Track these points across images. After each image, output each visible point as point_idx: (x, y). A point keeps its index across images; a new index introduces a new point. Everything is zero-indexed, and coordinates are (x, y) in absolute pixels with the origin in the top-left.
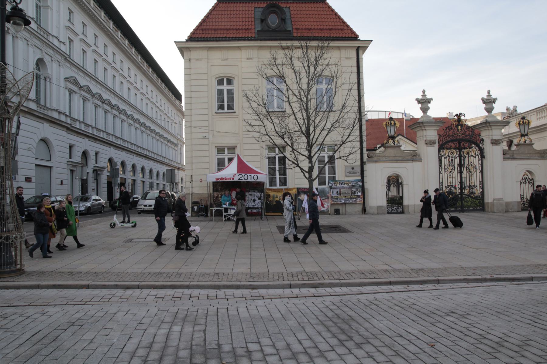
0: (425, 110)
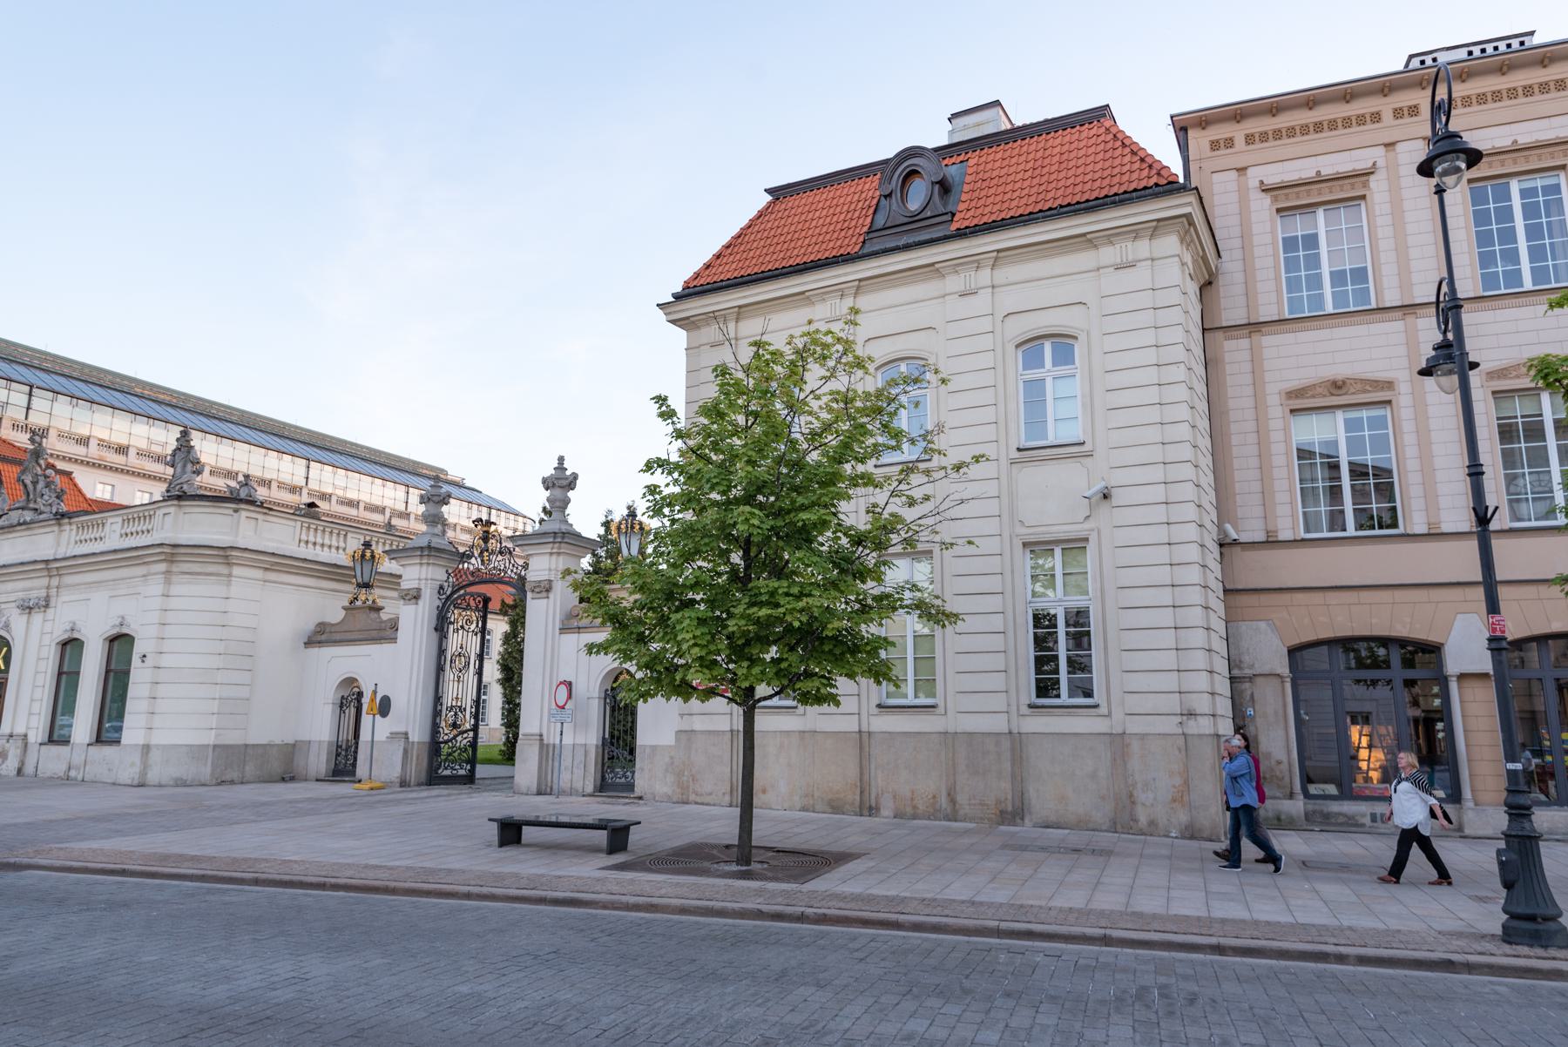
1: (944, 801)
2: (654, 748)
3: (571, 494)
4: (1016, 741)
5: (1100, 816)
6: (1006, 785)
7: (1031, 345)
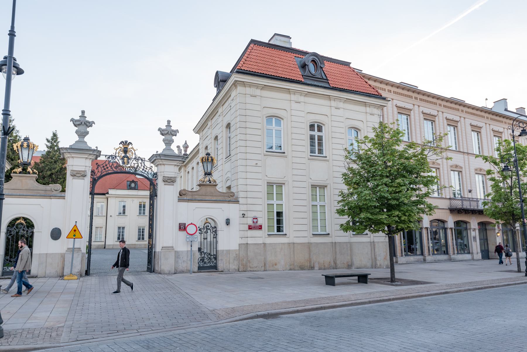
0: (82, 134)
1: (332, 263)
2: (228, 252)
3: (89, 129)
4: (350, 243)
5: (369, 264)
6: (349, 257)
7: (270, 117)
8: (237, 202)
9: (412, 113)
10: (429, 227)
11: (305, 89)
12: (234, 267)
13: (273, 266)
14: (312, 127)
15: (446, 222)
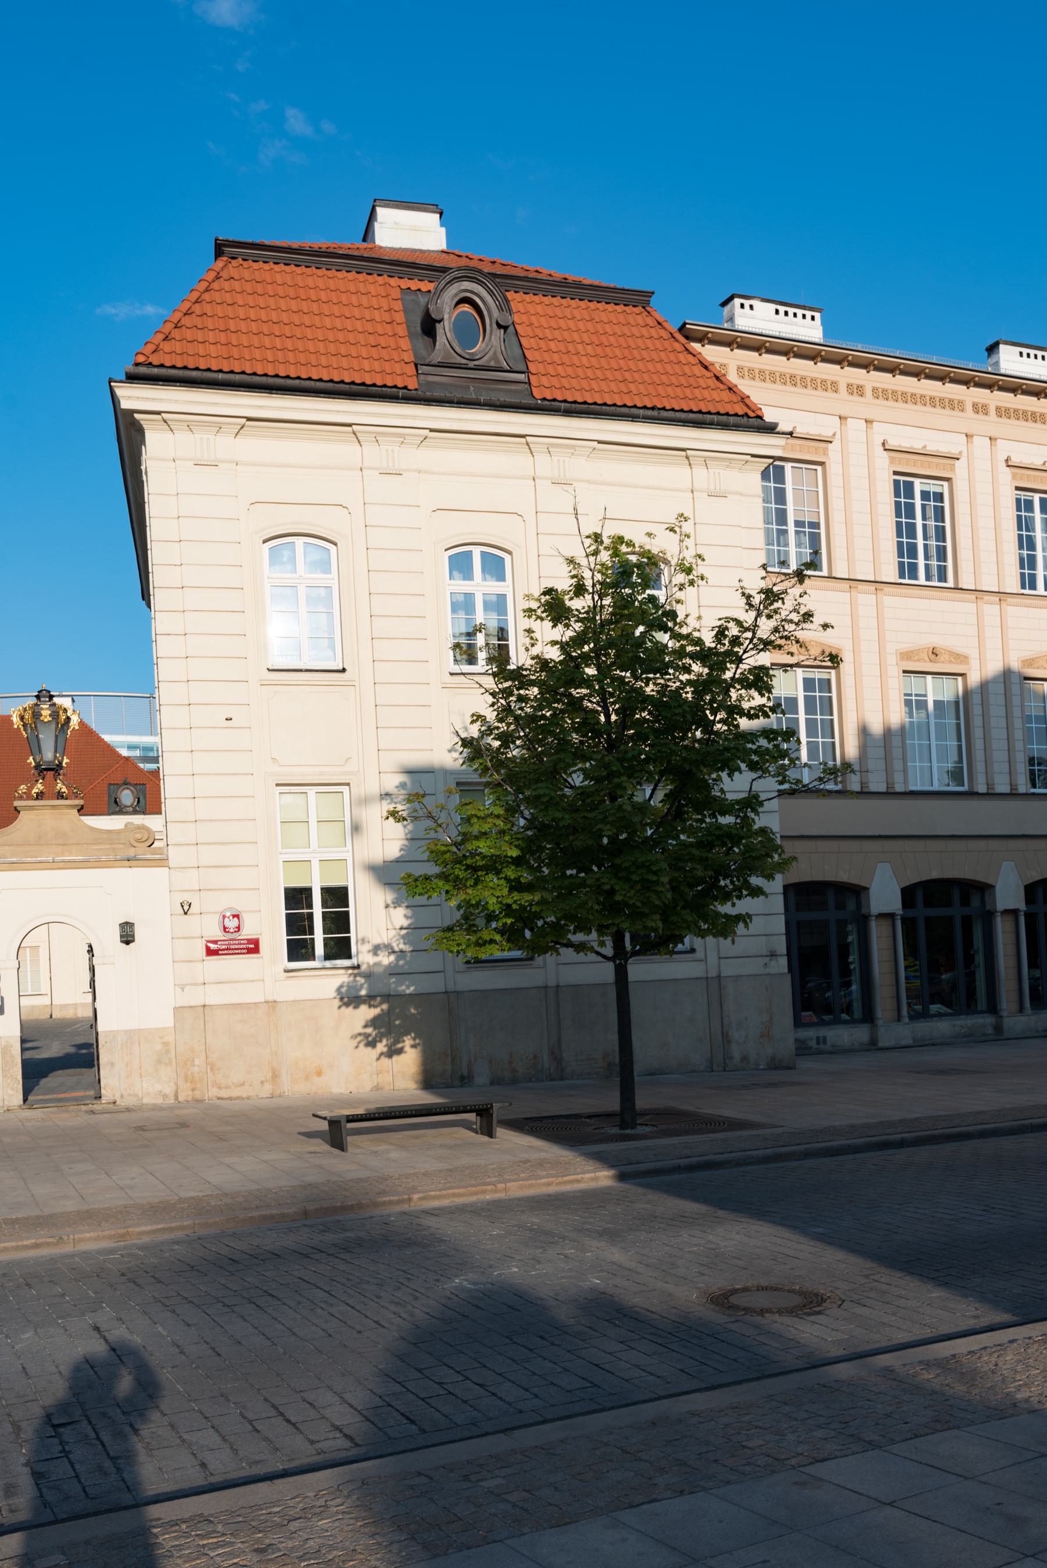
2: (132, 1036)
8: (162, 862)
9: (833, 455)
10: (1022, 906)
11: (414, 417)
12: (158, 1087)
13: (307, 1078)
14: (460, 564)
15: (866, 889)
